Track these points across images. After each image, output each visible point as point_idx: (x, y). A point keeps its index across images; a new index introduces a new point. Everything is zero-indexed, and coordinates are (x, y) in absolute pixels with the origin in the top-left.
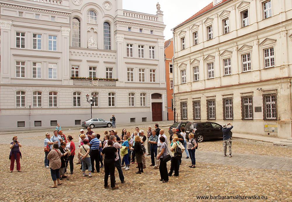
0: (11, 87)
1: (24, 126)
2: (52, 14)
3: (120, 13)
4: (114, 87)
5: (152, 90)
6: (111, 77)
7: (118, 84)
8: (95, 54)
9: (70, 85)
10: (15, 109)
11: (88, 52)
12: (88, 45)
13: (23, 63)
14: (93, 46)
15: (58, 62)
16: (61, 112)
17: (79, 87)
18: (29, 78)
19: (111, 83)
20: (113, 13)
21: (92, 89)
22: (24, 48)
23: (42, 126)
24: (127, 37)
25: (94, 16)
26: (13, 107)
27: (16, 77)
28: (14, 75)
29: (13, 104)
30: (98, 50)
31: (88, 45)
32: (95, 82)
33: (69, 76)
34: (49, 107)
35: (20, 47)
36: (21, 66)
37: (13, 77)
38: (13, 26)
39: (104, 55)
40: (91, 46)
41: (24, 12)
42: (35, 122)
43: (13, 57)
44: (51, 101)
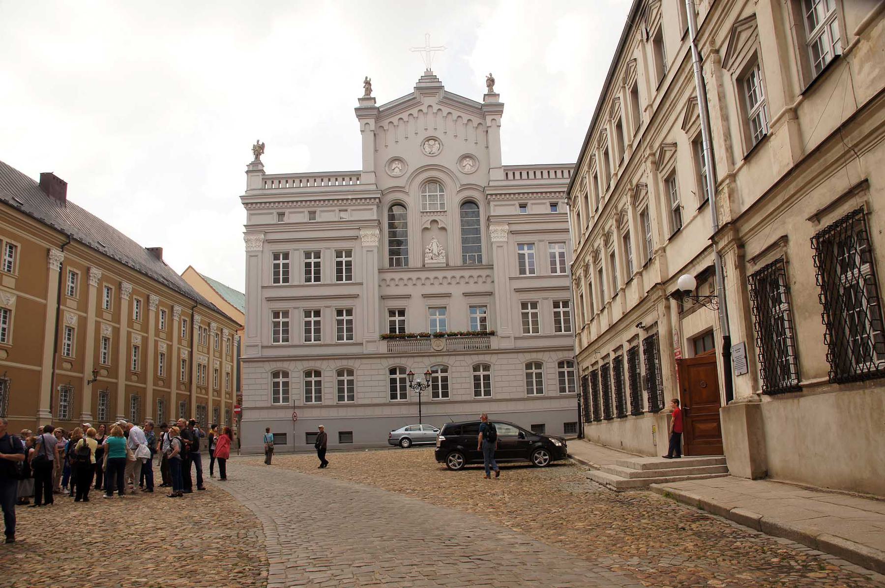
0: (378, 361)
1: (286, 444)
2: (309, 207)
3: (501, 175)
4: (488, 351)
5: (307, 362)
7: (494, 343)
8: (458, 278)
9: (380, 352)
10: (524, 400)
11: (423, 275)
12: (426, 259)
13: (286, 314)
14: (435, 261)
15: (354, 306)
17: (401, 357)
18: (328, 342)
19: (480, 342)
20: (479, 180)
21: (431, 358)
22: (351, 280)
24: (515, 228)
25: (438, 194)
26: (383, 401)
28: (269, 339)
29: (264, 398)
30: (448, 267)
31: (424, 260)
32: (438, 342)
33: (377, 336)
34: (526, 396)
35: (279, 283)
37: (265, 344)
38: (510, 235)
39: (436, 280)
40: (431, 261)
42: (308, 434)
44: (341, 390)
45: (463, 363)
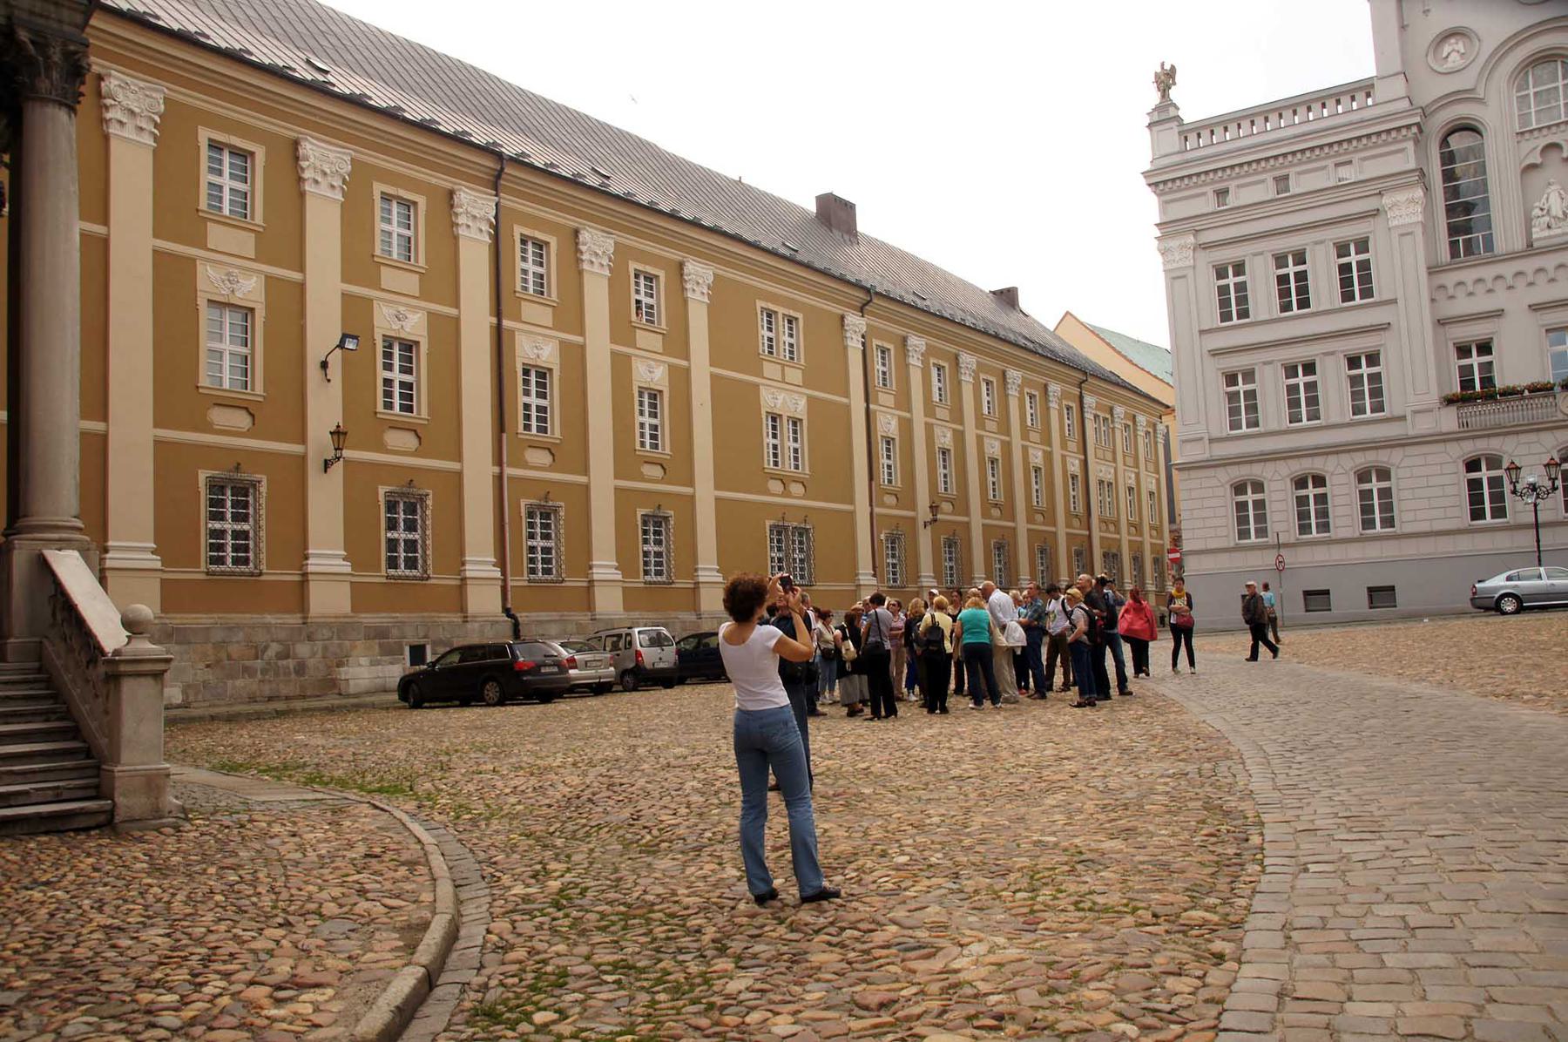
0: (1211, 472)
2: (1273, 168)
6: (1487, 381)
9: (1444, 430)
11: (1529, 265)
16: (1410, 549)
22: (1248, 317)
23: (1334, 611)
27: (1227, 432)
31: (1529, 233)
36: (1365, 370)
37: (1216, 434)
40: (1547, 233)
41: (1292, 171)
43: (1209, 361)
45: (1214, 482)
